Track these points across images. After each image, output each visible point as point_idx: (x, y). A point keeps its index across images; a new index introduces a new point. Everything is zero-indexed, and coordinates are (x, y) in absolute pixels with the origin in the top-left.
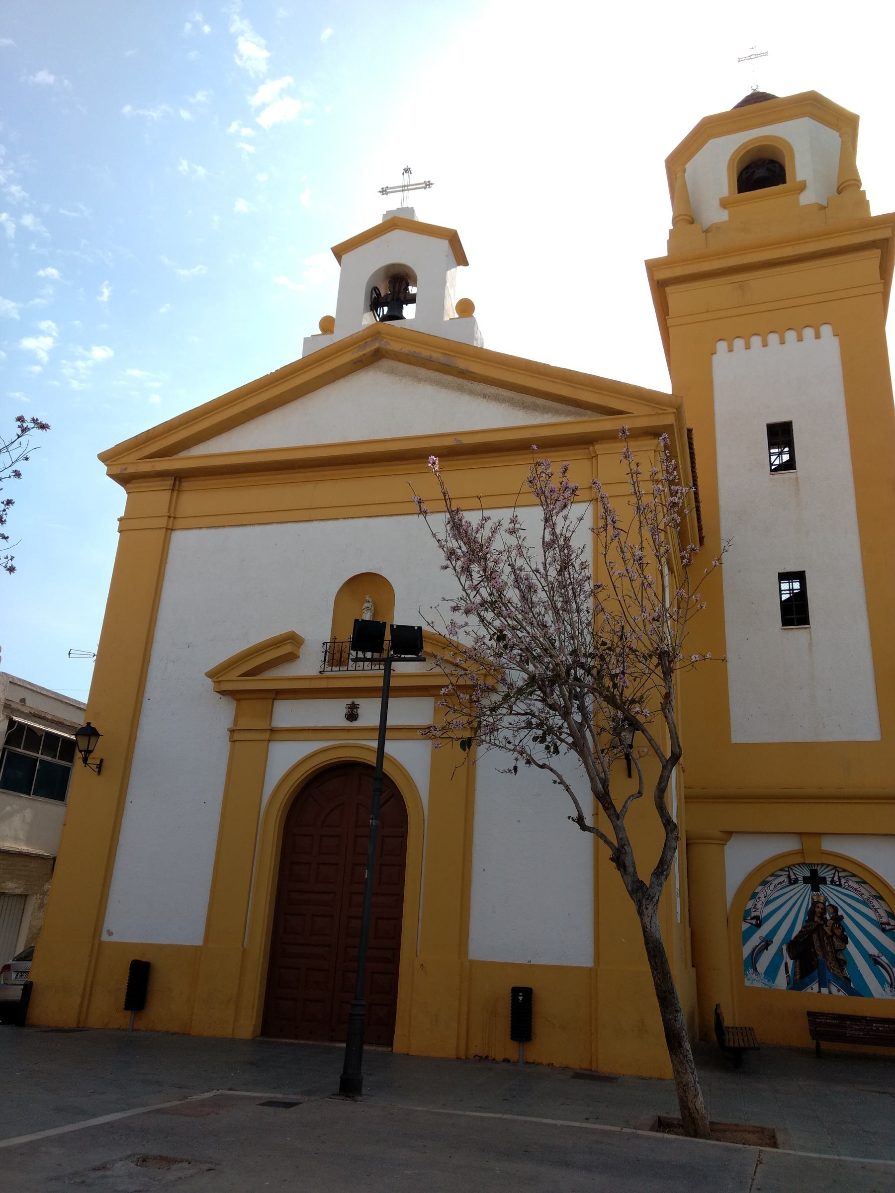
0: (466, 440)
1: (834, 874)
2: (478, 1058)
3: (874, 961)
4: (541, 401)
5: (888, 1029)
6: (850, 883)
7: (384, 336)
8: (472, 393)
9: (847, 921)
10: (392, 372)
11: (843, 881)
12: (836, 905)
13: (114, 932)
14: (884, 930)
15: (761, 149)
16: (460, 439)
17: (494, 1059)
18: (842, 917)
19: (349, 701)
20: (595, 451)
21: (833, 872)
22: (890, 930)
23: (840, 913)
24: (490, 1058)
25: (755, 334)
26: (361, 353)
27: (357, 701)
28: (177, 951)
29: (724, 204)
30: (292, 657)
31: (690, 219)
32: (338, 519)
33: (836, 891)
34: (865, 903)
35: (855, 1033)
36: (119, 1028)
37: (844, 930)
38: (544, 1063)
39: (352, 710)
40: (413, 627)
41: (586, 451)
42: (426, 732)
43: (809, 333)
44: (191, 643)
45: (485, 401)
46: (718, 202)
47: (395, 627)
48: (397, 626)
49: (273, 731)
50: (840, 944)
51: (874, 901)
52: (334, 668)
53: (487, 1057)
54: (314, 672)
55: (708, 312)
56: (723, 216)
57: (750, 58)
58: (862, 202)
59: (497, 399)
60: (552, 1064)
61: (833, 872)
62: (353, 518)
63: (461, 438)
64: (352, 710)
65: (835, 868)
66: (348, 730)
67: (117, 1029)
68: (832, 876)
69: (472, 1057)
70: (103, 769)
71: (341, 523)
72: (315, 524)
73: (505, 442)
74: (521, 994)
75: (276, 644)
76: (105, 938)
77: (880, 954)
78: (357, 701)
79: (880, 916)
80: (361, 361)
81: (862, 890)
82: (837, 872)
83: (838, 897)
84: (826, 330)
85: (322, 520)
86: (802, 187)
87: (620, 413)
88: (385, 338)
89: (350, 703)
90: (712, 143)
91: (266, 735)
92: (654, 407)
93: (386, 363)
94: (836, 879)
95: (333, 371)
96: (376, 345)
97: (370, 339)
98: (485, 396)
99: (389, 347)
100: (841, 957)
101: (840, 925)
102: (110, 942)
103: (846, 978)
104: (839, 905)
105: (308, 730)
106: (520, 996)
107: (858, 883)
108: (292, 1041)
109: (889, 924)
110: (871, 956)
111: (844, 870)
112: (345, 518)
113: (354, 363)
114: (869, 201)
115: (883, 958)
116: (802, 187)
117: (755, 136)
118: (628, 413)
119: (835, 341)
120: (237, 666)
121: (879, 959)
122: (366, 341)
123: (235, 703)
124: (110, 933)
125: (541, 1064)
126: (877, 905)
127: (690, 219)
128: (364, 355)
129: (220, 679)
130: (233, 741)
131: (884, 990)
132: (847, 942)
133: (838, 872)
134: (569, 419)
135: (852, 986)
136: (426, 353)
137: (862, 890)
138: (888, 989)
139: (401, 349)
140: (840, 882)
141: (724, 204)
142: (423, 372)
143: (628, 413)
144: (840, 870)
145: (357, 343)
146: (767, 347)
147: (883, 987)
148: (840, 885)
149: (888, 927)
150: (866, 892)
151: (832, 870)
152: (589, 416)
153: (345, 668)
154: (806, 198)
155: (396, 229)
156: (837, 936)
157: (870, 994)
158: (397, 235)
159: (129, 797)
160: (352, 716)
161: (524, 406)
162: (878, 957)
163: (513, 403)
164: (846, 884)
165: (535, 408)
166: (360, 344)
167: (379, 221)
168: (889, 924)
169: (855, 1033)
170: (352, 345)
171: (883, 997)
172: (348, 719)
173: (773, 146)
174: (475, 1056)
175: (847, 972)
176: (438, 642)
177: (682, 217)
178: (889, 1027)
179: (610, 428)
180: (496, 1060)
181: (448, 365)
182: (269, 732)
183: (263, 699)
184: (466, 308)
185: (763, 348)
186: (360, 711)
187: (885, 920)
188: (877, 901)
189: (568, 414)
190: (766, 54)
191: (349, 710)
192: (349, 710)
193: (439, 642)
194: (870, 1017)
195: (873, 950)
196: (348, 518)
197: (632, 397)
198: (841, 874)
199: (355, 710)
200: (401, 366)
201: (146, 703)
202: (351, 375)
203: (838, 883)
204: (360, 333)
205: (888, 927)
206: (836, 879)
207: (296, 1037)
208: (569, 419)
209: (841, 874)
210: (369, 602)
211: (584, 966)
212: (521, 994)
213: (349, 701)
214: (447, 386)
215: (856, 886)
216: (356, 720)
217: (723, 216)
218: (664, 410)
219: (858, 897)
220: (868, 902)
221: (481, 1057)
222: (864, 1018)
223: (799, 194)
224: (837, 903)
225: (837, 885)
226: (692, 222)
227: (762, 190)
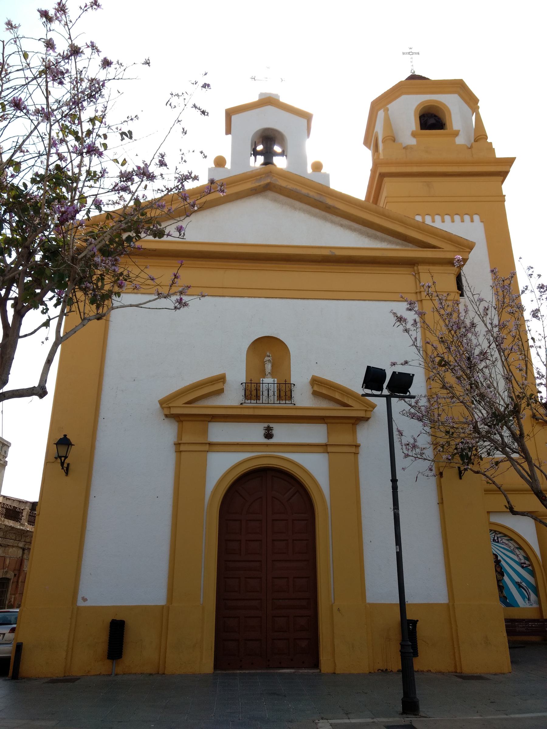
0: (338, 253)
1: (495, 536)
2: (380, 671)
3: (519, 586)
4: (379, 234)
5: (537, 625)
6: (504, 541)
7: (274, 175)
8: (332, 222)
9: (503, 563)
10: (275, 200)
11: (500, 539)
12: (496, 554)
13: (87, 599)
14: (523, 567)
15: (436, 107)
16: (333, 252)
17: (391, 671)
18: (500, 561)
19: (266, 425)
20: (418, 270)
21: (494, 534)
22: (526, 567)
23: (499, 558)
24: (389, 671)
25: (457, 214)
26: (257, 184)
27: (271, 425)
28: (144, 610)
29: (414, 135)
30: (220, 392)
31: (393, 138)
32: (244, 297)
33: (498, 546)
34: (512, 552)
35: (521, 629)
36: (99, 675)
37: (501, 568)
38: (425, 670)
39: (268, 431)
40: (409, 374)
41: (412, 269)
42: (324, 448)
43: (467, 218)
44: (136, 378)
45: (342, 229)
46: (410, 133)
47: (397, 373)
48: (399, 373)
49: (210, 444)
50: (500, 576)
51: (517, 550)
52: (287, 402)
53: (386, 670)
54: (236, 403)
55: (410, 197)
56: (413, 142)
57: (409, 53)
58: (490, 148)
59: (350, 228)
60: (430, 671)
61: (494, 534)
62: (255, 297)
63: (333, 251)
64: (268, 431)
65: (495, 531)
66: (267, 445)
67: (97, 675)
68: (493, 537)
69: (376, 671)
70: (70, 472)
71: (246, 300)
72: (227, 299)
73: (391, 258)
74: (411, 625)
75: (212, 382)
76: (80, 603)
77: (522, 581)
78: (271, 425)
79: (520, 559)
80: (256, 190)
81: (510, 544)
82: (496, 535)
83: (499, 550)
84: (476, 218)
85: (232, 297)
86: (456, 134)
87: (434, 247)
88: (274, 176)
89: (266, 426)
90: (404, 98)
91: (206, 448)
92: (457, 247)
93: (271, 194)
94: (496, 538)
95: (237, 193)
96: (268, 181)
97: (264, 176)
98: (342, 225)
99: (278, 183)
100: (501, 584)
101: (499, 566)
102: (85, 607)
103: (504, 596)
104: (499, 554)
105: (238, 444)
106: (411, 626)
107: (508, 540)
108: (244, 671)
109: (525, 564)
110: (516, 582)
111: (500, 533)
112: (249, 297)
113: (251, 190)
114: (494, 149)
115: (523, 583)
116: (456, 134)
117: (429, 99)
118: (440, 248)
119: (482, 225)
120: (184, 395)
121: (521, 584)
122: (261, 176)
123: (177, 424)
124: (85, 600)
125: (423, 671)
126: (518, 553)
127: (393, 138)
128: (260, 185)
129: (170, 405)
130: (179, 452)
131: (525, 602)
132: (504, 576)
133: (497, 534)
134: (398, 247)
135: (508, 601)
136: (304, 191)
137: (510, 544)
138: (527, 602)
139: (287, 186)
140: (498, 540)
141: (414, 135)
142: (297, 204)
143: (440, 248)
144: (497, 533)
145: (255, 176)
146: (434, 223)
147: (524, 601)
148: (498, 542)
149: (525, 565)
150: (512, 545)
151: (494, 533)
152: (410, 247)
153: (284, 402)
154: (460, 140)
155: (270, 105)
156: (498, 572)
157: (518, 606)
158: (269, 109)
159: (93, 493)
160: (269, 435)
161: (369, 236)
162: (521, 583)
163: (361, 233)
164: (502, 541)
165: (376, 238)
166: (258, 177)
167: (255, 98)
168: (525, 564)
169: (521, 629)
170: (251, 178)
171: (525, 607)
172: (266, 437)
173: (425, 107)
174: (378, 670)
175: (505, 593)
176: (331, 386)
177: (388, 138)
178: (537, 624)
179: (430, 257)
180: (393, 672)
181: (321, 202)
182: (208, 445)
183: (190, 421)
184: (317, 167)
185: (452, 223)
186: (274, 432)
187: (523, 561)
188: (518, 550)
189: (397, 244)
190: (403, 53)
191: (267, 431)
192: (267, 431)
193: (332, 387)
194: (527, 619)
195: (518, 579)
196: (251, 297)
197: (445, 239)
198: (498, 536)
199: (270, 431)
200: (282, 198)
201: (101, 420)
202: (246, 198)
203: (497, 541)
204: (258, 170)
205: (525, 565)
206: (496, 538)
207: (241, 668)
208: (398, 247)
209: (498, 536)
210: (269, 356)
211: (443, 602)
212: (411, 625)
213: (266, 425)
214: (315, 215)
215: (507, 542)
216: (272, 438)
217: (413, 142)
218: (463, 249)
219: (507, 548)
220: (513, 551)
221: (382, 671)
222: (524, 620)
223: (455, 137)
224: (498, 553)
225: (496, 542)
226: (394, 141)
227: (436, 130)
